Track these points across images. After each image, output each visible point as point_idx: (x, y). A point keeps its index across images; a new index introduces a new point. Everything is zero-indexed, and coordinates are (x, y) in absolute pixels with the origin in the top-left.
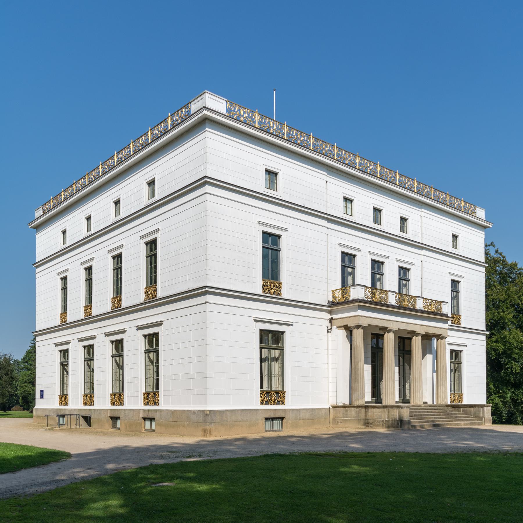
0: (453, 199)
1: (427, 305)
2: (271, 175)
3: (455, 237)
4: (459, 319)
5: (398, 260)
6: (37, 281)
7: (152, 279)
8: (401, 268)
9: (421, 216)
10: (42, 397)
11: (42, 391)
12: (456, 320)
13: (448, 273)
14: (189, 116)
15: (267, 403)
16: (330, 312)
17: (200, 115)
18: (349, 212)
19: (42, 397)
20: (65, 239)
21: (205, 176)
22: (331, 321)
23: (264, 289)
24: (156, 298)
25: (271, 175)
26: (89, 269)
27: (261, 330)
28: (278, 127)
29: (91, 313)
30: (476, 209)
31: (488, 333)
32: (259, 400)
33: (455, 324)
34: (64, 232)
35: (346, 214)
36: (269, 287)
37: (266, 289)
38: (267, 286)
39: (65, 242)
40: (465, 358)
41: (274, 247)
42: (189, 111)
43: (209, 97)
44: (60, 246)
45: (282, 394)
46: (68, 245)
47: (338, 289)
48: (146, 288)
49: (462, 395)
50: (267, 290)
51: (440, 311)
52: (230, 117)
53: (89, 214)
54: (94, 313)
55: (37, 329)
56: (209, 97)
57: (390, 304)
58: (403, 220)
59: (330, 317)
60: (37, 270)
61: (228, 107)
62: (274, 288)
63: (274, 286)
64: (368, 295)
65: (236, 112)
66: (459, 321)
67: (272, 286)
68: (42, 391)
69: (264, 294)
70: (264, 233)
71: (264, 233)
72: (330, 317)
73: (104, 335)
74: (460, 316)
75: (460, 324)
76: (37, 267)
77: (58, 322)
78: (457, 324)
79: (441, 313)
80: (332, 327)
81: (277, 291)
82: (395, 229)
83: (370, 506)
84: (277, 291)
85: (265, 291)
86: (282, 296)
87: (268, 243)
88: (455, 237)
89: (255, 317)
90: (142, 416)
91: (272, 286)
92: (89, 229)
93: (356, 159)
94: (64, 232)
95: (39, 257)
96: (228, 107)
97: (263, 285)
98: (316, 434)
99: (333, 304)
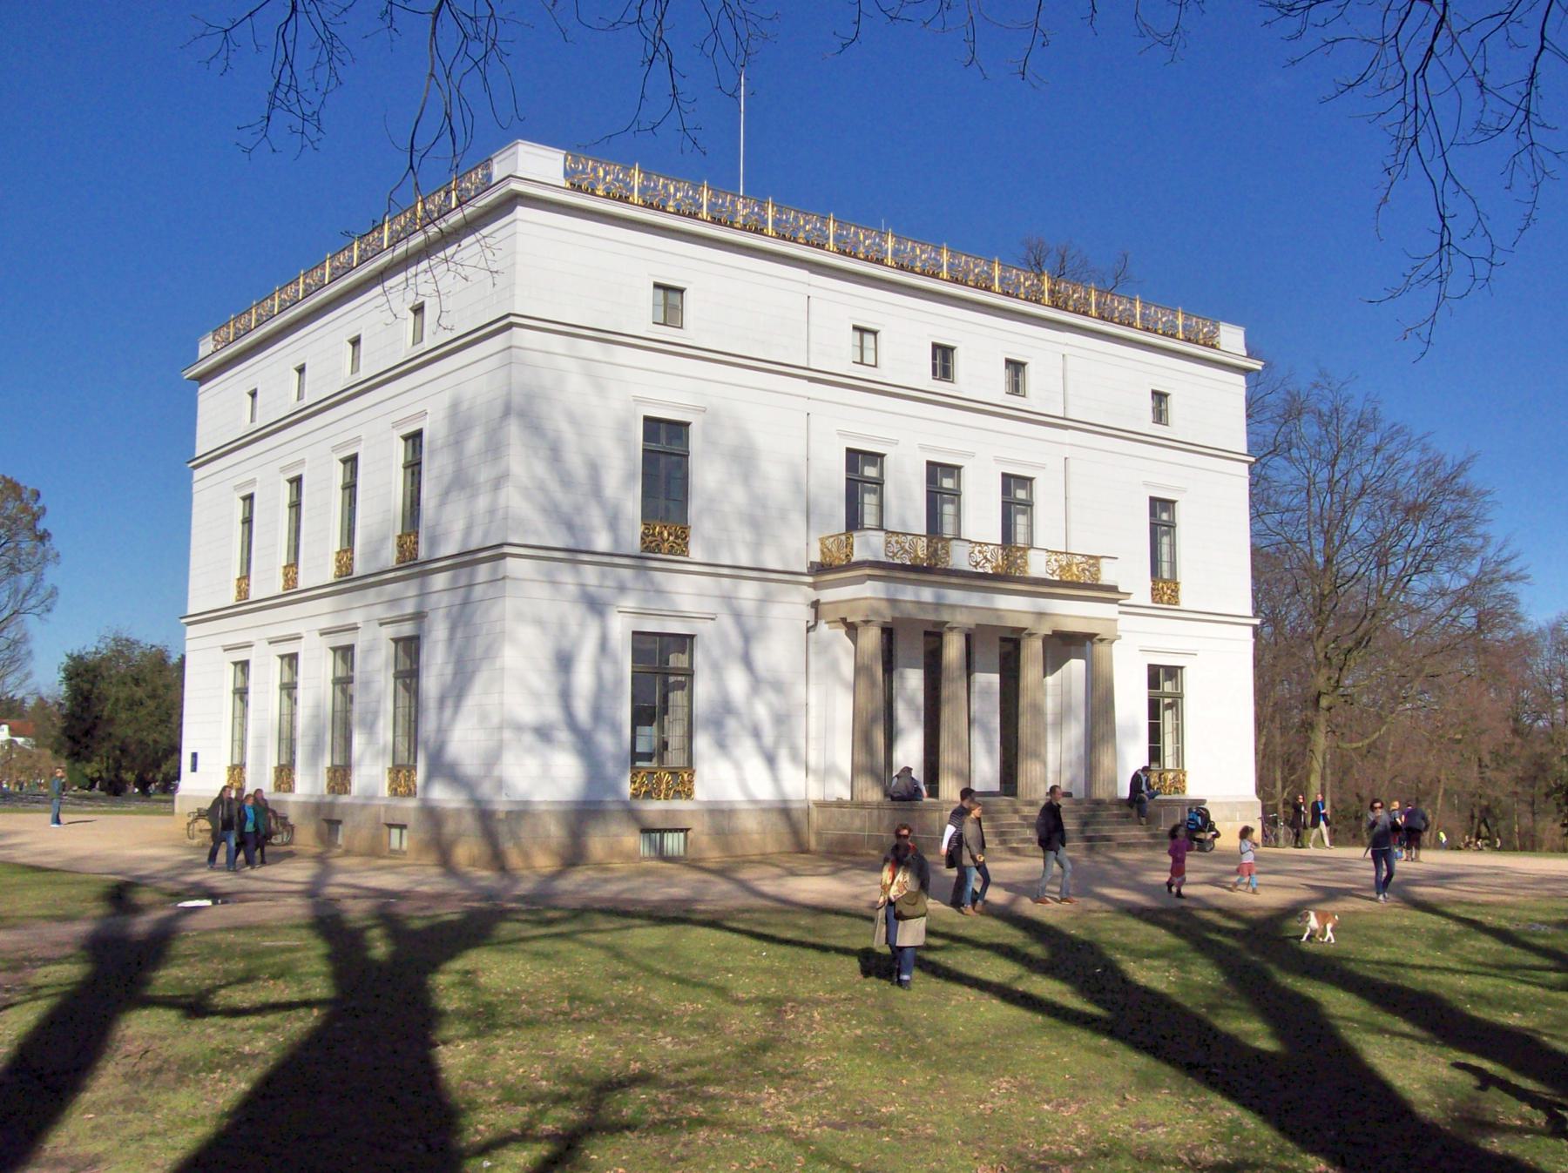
0: (1153, 309)
1: (1060, 566)
2: (670, 294)
3: (1159, 397)
4: (1175, 591)
5: (998, 460)
6: (197, 499)
7: (293, 565)
9: (1064, 356)
10: (194, 769)
11: (195, 756)
12: (1164, 594)
14: (487, 186)
16: (815, 586)
17: (503, 190)
18: (869, 358)
19: (194, 769)
20: (355, 362)
22: (816, 605)
24: (416, 559)
25: (670, 294)
26: (351, 462)
28: (688, 193)
29: (295, 580)
30: (1218, 329)
31: (1257, 622)
34: (356, 342)
35: (862, 363)
36: (659, 538)
37: (651, 542)
38: (653, 535)
39: (355, 367)
41: (676, 448)
42: (489, 176)
43: (527, 152)
44: (244, 426)
46: (307, 401)
47: (832, 536)
48: (400, 537)
50: (653, 544)
51: (1098, 579)
52: (575, 187)
53: (356, 334)
54: (302, 585)
55: (190, 613)
56: (527, 152)
57: (955, 567)
58: (1016, 367)
59: (813, 595)
60: (198, 474)
61: (571, 167)
62: (671, 538)
63: (670, 534)
64: (896, 551)
65: (588, 174)
66: (1176, 597)
67: (666, 534)
68: (195, 756)
72: (813, 595)
73: (317, 633)
74: (1176, 584)
75: (1177, 603)
76: (195, 467)
77: (231, 598)
78: (1169, 604)
79: (1100, 582)
80: (816, 623)
81: (679, 545)
82: (994, 387)
83: (102, 1120)
85: (646, 548)
86: (690, 555)
87: (657, 441)
88: (1159, 397)
91: (666, 534)
92: (354, 369)
93: (886, 242)
94: (356, 342)
95: (201, 448)
96: (571, 167)
99: (819, 569)
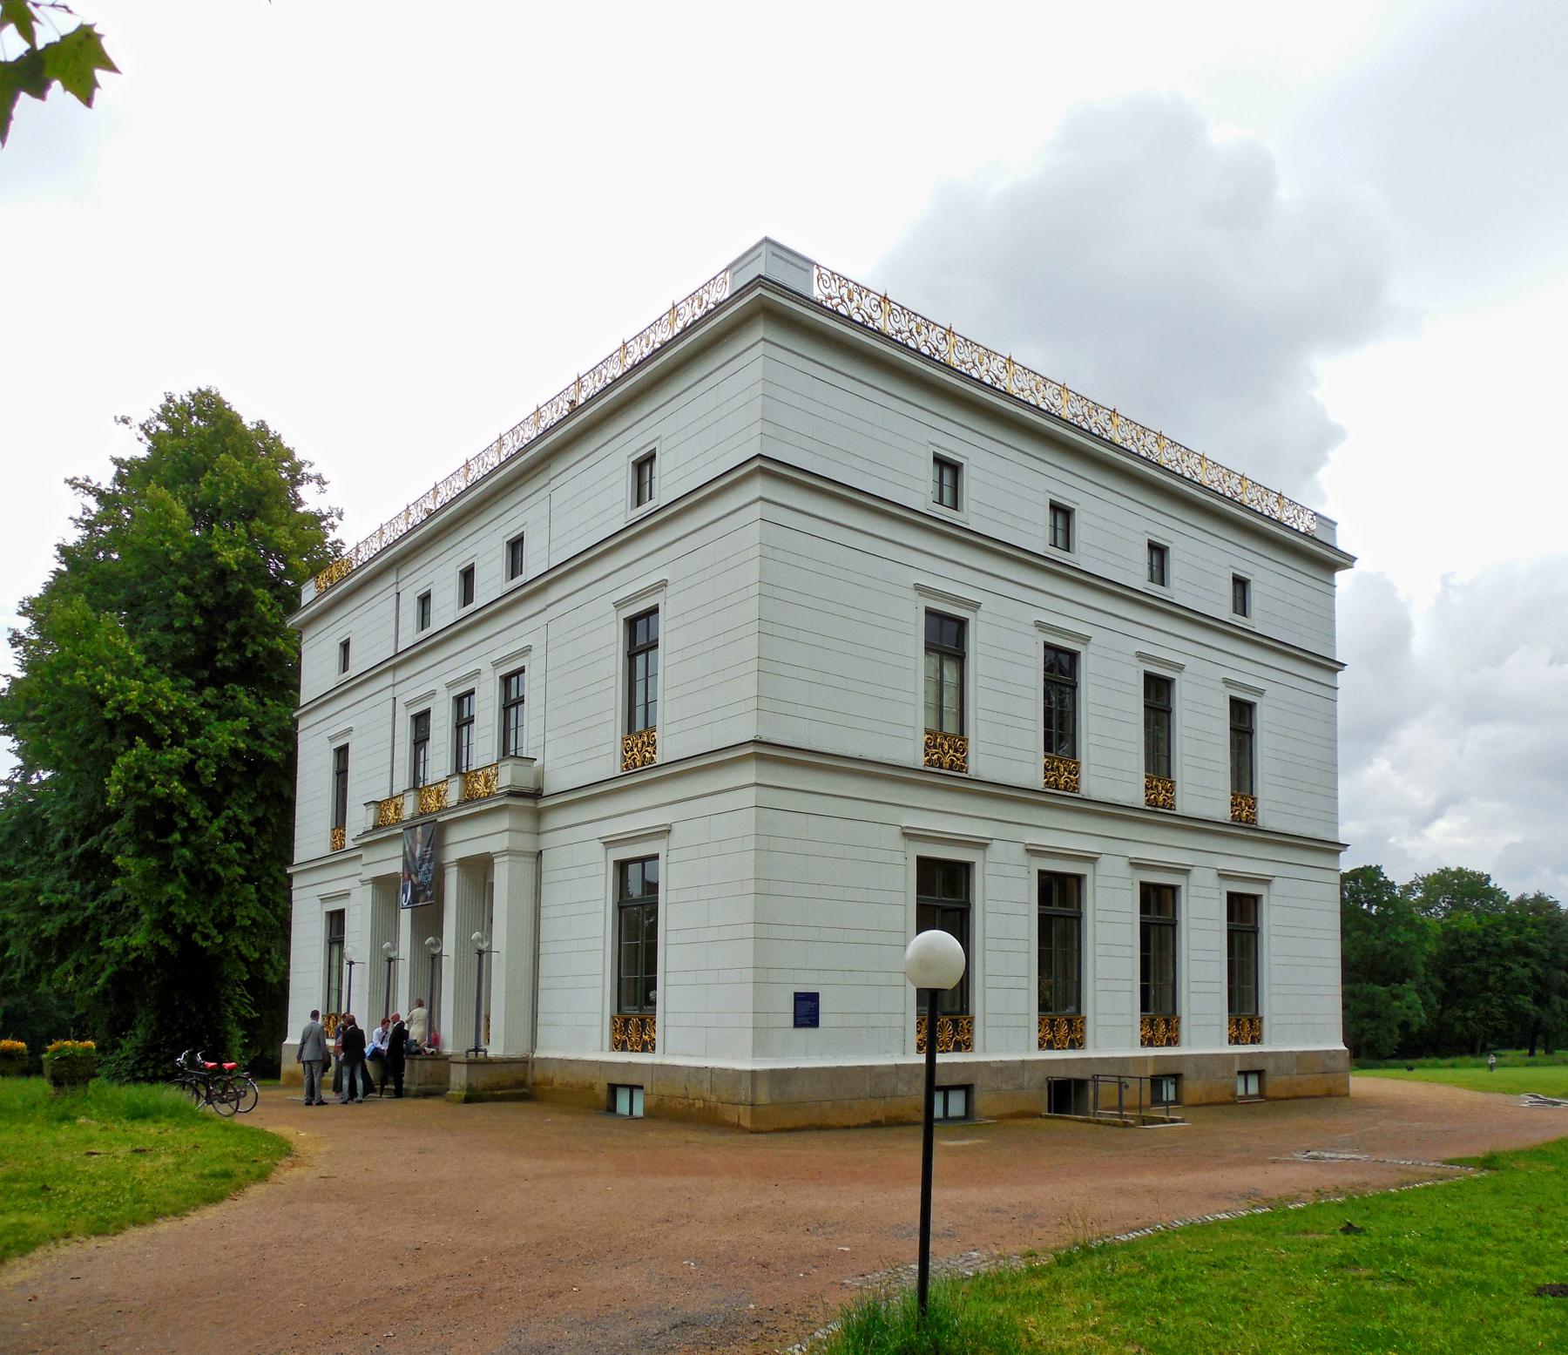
8: (1149, 677)
13: (912, 586)
15: (1150, 1044)
21: (759, 455)
23: (927, 755)
27: (1143, 884)
32: (1138, 1035)
33: (1057, 788)
37: (933, 755)
40: (1272, 920)
45: (965, 1023)
49: (1261, 1020)
63: (950, 747)
67: (946, 747)
69: (1148, 808)
70: (929, 612)
71: (929, 612)
81: (958, 759)
84: (958, 759)
85: (929, 761)
86: (970, 772)
88: (1240, 584)
89: (907, 827)
90: (1237, 1068)
97: (926, 744)
98: (652, 1135)
